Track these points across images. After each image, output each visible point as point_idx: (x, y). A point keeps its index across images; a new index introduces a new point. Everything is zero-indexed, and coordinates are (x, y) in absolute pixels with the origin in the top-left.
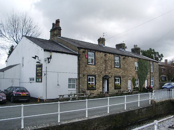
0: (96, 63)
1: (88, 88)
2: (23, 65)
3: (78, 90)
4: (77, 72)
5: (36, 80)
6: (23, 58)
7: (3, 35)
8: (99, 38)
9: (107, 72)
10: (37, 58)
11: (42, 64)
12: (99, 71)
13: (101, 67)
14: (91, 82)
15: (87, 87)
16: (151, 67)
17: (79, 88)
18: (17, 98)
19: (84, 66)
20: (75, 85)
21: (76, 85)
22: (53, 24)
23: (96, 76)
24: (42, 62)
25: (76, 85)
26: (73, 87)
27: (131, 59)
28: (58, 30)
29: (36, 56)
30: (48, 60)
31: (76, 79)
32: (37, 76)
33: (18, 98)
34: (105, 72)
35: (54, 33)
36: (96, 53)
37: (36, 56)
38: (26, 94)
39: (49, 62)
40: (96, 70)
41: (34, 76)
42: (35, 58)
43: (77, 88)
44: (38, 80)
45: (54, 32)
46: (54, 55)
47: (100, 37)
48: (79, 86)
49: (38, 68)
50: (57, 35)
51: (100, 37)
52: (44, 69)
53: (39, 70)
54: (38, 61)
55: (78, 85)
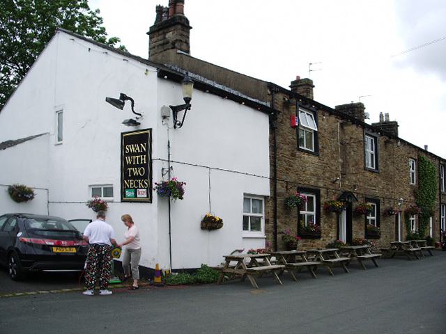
0: (320, 146)
1: (299, 230)
2: (60, 139)
3: (271, 235)
4: (266, 171)
5: (123, 194)
6: (60, 113)
8: (294, 79)
9: (347, 183)
10: (128, 103)
11: (151, 130)
12: (328, 178)
13: (332, 162)
14: (251, 214)
15: (296, 229)
17: (273, 231)
18: (36, 264)
20: (260, 218)
21: (263, 222)
22: (160, 10)
23: (321, 192)
24: (151, 121)
25: (263, 222)
26: (256, 226)
27: (402, 148)
28: (179, 27)
30: (175, 116)
31: (266, 197)
32: (125, 175)
33: (39, 263)
34: (343, 181)
35: (165, 38)
37: (124, 97)
38: (76, 247)
39: (181, 125)
40: (320, 172)
41: (112, 175)
42: (119, 103)
43: (267, 231)
44: (129, 194)
45: (165, 34)
46: (198, 98)
47: (298, 77)
48: (275, 223)
49: (132, 148)
50: (177, 45)
51: (298, 77)
52: (158, 151)
53: (138, 154)
54: (133, 117)
55: (271, 219)
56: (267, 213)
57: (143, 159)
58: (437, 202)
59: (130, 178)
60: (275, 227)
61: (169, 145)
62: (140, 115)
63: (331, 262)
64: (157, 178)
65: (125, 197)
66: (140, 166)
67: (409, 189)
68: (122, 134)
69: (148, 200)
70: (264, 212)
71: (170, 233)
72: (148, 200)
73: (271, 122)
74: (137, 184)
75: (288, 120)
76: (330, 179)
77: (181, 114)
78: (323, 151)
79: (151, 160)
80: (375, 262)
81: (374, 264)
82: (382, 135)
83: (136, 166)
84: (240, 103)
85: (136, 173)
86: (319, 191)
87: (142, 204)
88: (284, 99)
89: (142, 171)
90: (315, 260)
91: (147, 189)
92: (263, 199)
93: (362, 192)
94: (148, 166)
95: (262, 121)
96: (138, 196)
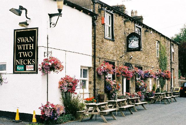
3: (92, 92)
7: (103, 77)
10: (24, 12)
16: (159, 48)
19: (100, 40)
29: (21, 8)
31: (89, 68)
36: (38, 46)
37: (21, 8)
39: (55, 25)
42: (19, 11)
43: (90, 89)
46: (66, 10)
52: (41, 41)
55: (93, 82)
56: (90, 77)
57: (32, 46)
58: (169, 68)
59: (21, 58)
60: (95, 86)
61: (48, 38)
62: (30, 19)
63: (123, 108)
64: (41, 59)
65: (16, 70)
66: (29, 50)
67: (156, 60)
68: (15, 30)
69: (35, 71)
70: (88, 77)
71: (47, 92)
72: (35, 71)
73: (93, 22)
74: (26, 62)
75: (100, 20)
76: (119, 55)
77: (54, 19)
78: (116, 39)
79: (37, 47)
80: (175, 100)
81: (143, 108)
82: (143, 27)
83: (26, 51)
84: (80, 11)
85: (25, 55)
86: (114, 63)
87: (21, 74)
88: (99, 7)
89: (30, 54)
90: (113, 107)
91: (34, 65)
92: (88, 69)
93: (134, 62)
94: (35, 50)
95: (89, 19)
96: (27, 70)
